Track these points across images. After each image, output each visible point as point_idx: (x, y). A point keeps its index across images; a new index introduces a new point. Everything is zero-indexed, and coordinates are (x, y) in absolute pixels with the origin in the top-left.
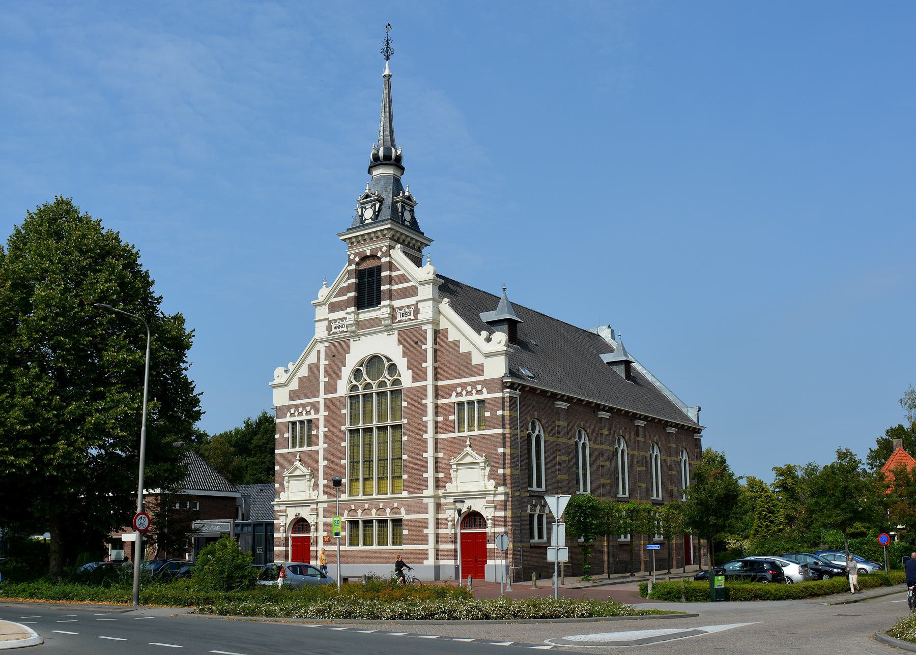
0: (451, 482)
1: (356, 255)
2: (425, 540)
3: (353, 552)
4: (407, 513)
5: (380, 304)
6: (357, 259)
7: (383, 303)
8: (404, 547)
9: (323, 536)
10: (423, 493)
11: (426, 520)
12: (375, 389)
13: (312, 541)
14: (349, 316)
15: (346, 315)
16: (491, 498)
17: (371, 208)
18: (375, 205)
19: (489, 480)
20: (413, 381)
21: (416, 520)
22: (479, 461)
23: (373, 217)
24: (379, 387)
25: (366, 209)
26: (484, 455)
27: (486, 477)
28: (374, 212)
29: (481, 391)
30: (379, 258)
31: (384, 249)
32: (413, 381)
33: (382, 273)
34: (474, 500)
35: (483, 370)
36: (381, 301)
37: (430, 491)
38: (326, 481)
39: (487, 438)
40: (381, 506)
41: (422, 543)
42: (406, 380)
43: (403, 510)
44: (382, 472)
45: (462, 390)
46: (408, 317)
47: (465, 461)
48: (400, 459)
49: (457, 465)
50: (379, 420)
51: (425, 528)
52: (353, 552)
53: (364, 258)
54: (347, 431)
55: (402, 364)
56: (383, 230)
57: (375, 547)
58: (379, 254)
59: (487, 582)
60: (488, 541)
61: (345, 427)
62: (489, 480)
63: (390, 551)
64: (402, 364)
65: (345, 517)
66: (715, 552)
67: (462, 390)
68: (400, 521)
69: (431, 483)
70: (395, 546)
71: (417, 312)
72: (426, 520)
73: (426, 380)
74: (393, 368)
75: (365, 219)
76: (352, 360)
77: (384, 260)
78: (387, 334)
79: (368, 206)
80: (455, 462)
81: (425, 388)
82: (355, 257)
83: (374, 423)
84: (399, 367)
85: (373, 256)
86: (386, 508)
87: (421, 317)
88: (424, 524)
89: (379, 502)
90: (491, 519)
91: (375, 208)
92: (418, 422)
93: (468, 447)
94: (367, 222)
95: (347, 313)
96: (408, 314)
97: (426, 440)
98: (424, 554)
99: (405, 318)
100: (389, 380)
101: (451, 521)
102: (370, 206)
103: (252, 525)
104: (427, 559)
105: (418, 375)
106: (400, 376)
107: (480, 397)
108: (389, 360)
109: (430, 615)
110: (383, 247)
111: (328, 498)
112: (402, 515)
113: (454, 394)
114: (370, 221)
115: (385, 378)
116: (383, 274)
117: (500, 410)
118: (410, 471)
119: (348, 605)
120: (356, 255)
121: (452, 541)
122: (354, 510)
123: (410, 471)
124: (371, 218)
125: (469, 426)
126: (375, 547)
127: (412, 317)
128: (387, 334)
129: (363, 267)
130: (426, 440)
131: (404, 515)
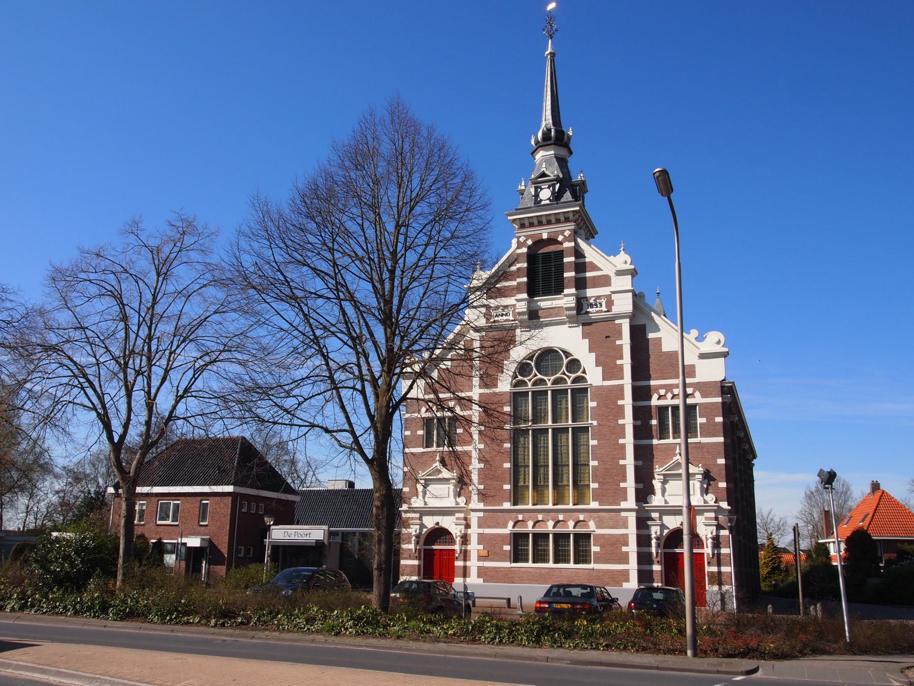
1: (527, 237)
2: (624, 559)
3: (522, 569)
4: (598, 527)
5: (563, 291)
7: (566, 291)
8: (592, 566)
9: (478, 550)
11: (626, 536)
13: (457, 555)
14: (518, 304)
15: (515, 302)
18: (554, 186)
20: (604, 379)
23: (551, 198)
24: (533, 386)
25: (542, 189)
26: (700, 465)
28: (553, 193)
29: (665, 395)
30: (561, 243)
31: (567, 233)
32: (604, 379)
33: (564, 259)
35: (694, 372)
36: (564, 289)
39: (702, 447)
41: (620, 563)
42: (594, 376)
45: (666, 393)
46: (597, 309)
50: (554, 421)
52: (522, 569)
55: (588, 360)
57: (551, 564)
58: (560, 238)
60: (457, 558)
64: (588, 360)
65: (509, 529)
66: (193, 572)
67: (666, 393)
68: (587, 536)
71: (610, 303)
72: (626, 536)
73: (622, 378)
74: (574, 365)
75: (541, 200)
76: (518, 353)
77: (567, 245)
79: (545, 186)
81: (621, 388)
84: (583, 363)
85: (552, 241)
86: (569, 520)
87: (616, 309)
88: (624, 540)
91: (554, 189)
92: (612, 425)
93: (678, 456)
94: (543, 203)
95: (517, 300)
96: (599, 306)
97: (623, 446)
98: (625, 575)
99: (594, 309)
100: (536, 375)
102: (547, 186)
103: (340, 534)
104: (627, 580)
105: (611, 371)
106: (584, 372)
108: (567, 354)
109: (672, 650)
110: (565, 230)
111: (600, 505)
112: (592, 529)
114: (548, 202)
115: (564, 374)
116: (566, 260)
117: (719, 416)
119: (462, 628)
121: (416, 557)
122: (583, 521)
124: (549, 199)
125: (674, 433)
126: (551, 564)
127: (604, 308)
130: (623, 446)
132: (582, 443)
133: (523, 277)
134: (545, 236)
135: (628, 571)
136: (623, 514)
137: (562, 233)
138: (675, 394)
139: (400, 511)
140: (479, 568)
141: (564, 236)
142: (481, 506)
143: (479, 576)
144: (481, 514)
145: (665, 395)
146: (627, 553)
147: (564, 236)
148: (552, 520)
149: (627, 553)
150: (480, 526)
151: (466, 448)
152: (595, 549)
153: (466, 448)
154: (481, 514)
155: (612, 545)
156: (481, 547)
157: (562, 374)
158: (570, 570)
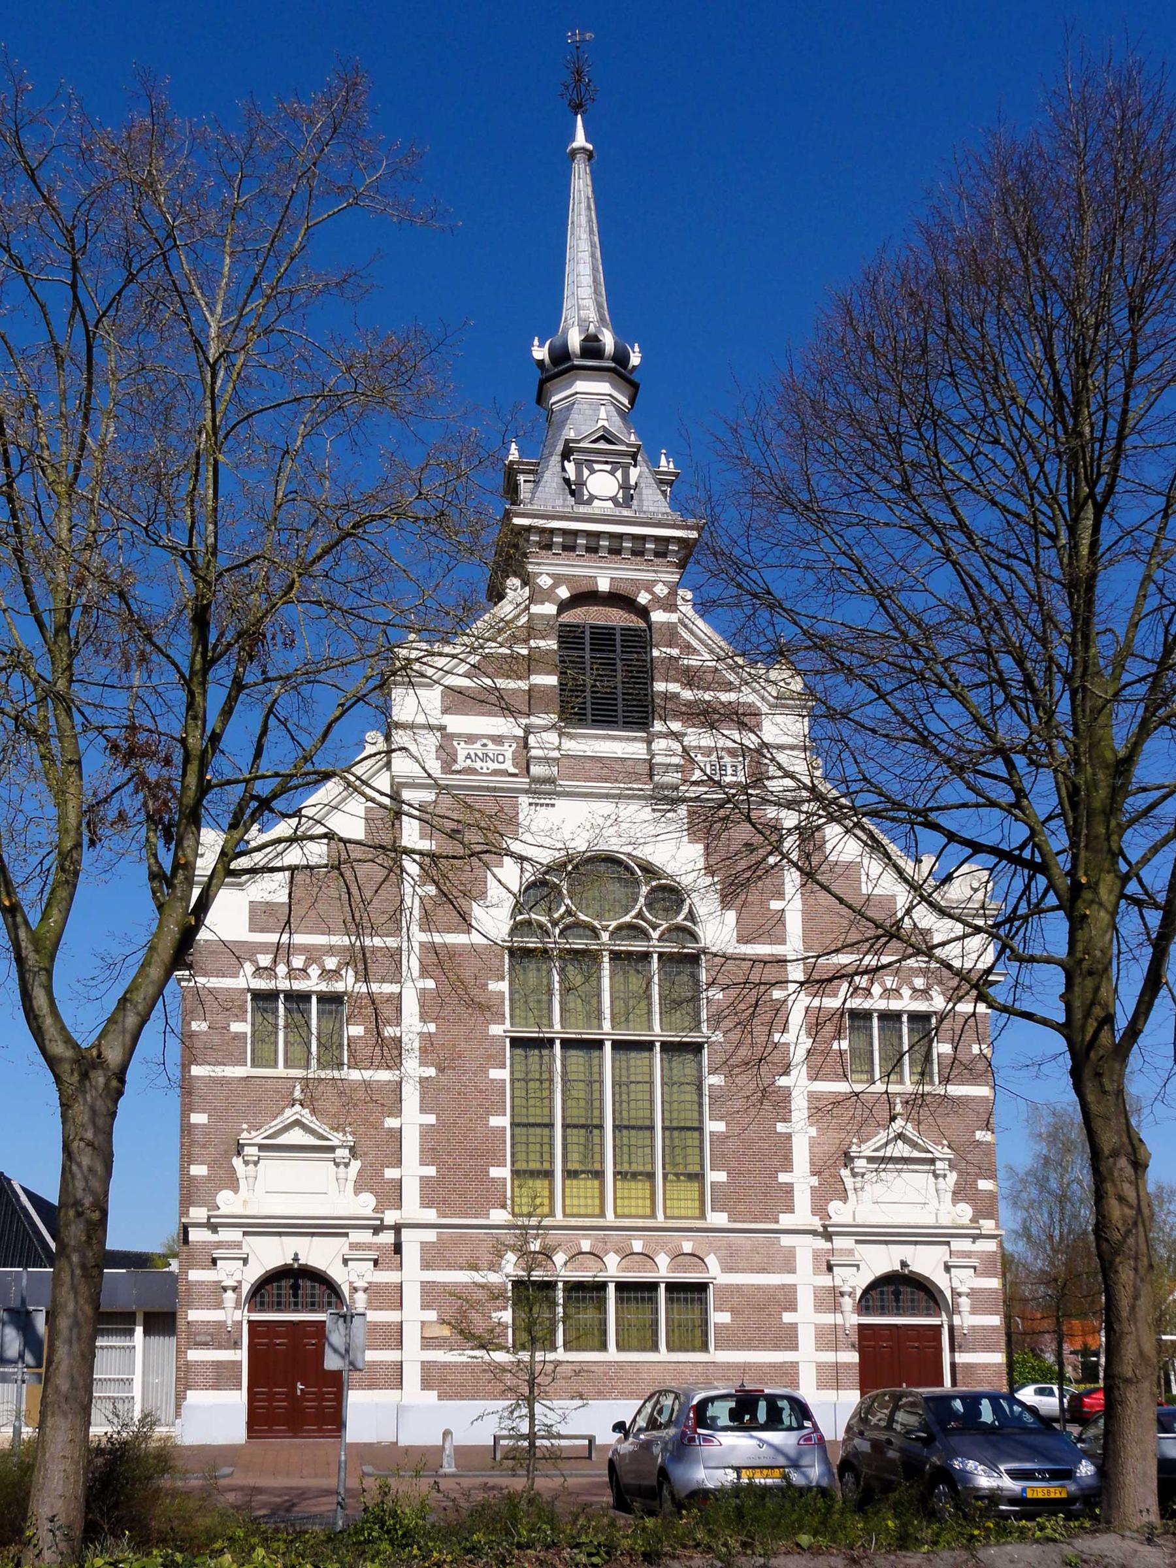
0: (845, 1199)
4: (728, 1269)
6: (564, 593)
10: (777, 1222)
12: (655, 943)
16: (366, 1236)
17: (612, 473)
19: (356, 1192)
20: (742, 940)
21: (758, 1287)
22: (336, 1142)
27: (350, 1185)
29: (304, 970)
34: (277, 1238)
37: (802, 1215)
38: (434, 1168)
40: (638, 1246)
41: (776, 1347)
43: (712, 1261)
44: (626, 1157)
47: (283, 1140)
48: (518, 1125)
49: (262, 1147)
51: (786, 1309)
53: (586, 597)
54: (508, 1040)
56: (621, 536)
57: (612, 1354)
59: (367, 1451)
61: (502, 1027)
62: (356, 1192)
63: (671, 1367)
69: (803, 1199)
70: (575, 1354)
78: (531, 800)
80: (259, 1140)
82: (555, 586)
83: (607, 1026)
89: (630, 1238)
90: (365, 1290)
101: (234, 1289)
107: (921, 1006)
111: (732, 1219)
113: (249, 968)
118: (734, 1164)
120: (558, 580)
123: (734, 1164)
126: (612, 1354)
128: (531, 800)
129: (572, 617)
131: (714, 1272)
132: (632, 1062)
133: (549, 673)
134: (604, 585)
135: (795, 1365)
136: (786, 1240)
137: (649, 586)
138: (328, 968)
139: (158, 1490)
140: (426, 1366)
141: (652, 593)
142: (431, 1215)
143: (426, 1384)
144: (431, 1235)
145: (304, 970)
146: (793, 1327)
147: (652, 593)
148: (616, 1252)
149: (793, 1327)
150: (426, 1265)
151: (829, 1357)
152: (719, 1317)
153: (829, 1357)
154: (431, 1235)
155: (760, 1308)
156: (432, 1315)
157: (636, 917)
158: (660, 1367)
